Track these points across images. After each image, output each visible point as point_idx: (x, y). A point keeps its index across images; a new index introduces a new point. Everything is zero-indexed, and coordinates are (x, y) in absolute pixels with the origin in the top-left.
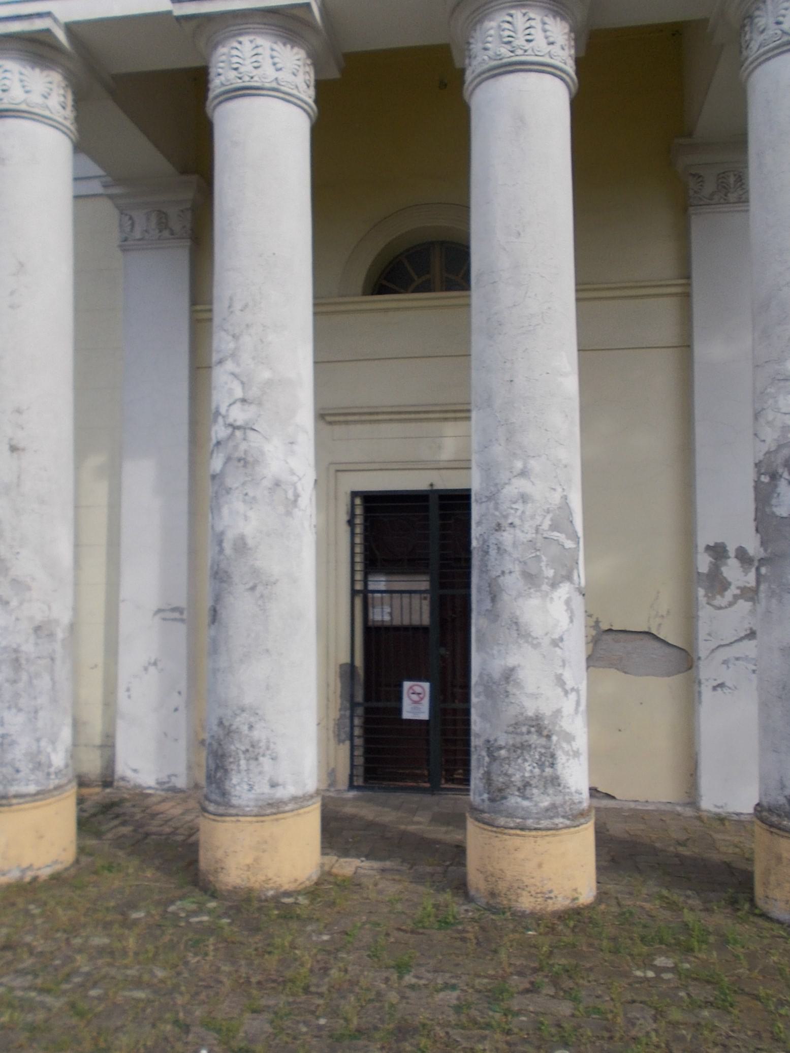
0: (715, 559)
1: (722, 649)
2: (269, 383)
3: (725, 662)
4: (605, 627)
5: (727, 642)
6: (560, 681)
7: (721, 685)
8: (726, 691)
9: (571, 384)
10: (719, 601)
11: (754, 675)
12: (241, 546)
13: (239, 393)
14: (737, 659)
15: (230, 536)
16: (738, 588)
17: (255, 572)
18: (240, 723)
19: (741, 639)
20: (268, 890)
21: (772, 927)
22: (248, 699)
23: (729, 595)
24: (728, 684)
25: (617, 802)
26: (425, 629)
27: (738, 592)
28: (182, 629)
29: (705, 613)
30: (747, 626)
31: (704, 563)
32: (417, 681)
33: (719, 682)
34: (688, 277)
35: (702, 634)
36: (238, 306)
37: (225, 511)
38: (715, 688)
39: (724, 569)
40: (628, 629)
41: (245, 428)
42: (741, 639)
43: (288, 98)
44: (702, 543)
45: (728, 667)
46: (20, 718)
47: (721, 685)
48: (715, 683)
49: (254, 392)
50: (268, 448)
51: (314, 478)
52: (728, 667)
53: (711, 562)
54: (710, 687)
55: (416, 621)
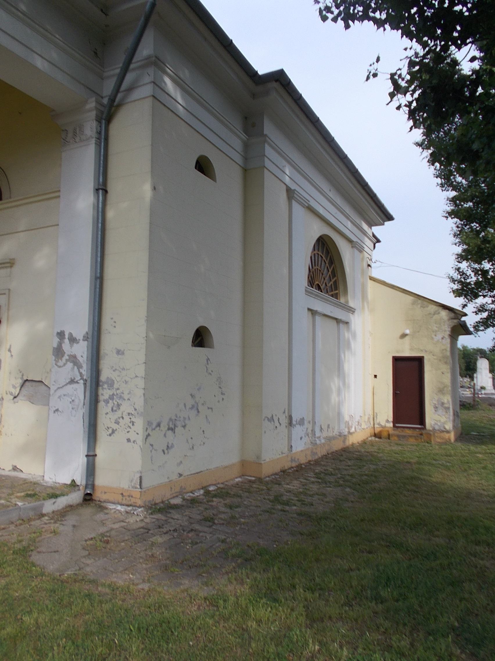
0: (60, 339)
1: (59, 390)
3: (59, 397)
4: (25, 378)
5: (61, 386)
7: (57, 410)
8: (59, 413)
10: (61, 363)
11: (70, 405)
14: (64, 395)
16: (68, 355)
19: (66, 385)
20: (477, 374)
24: (60, 409)
25: (24, 474)
27: (67, 358)
30: (70, 377)
32: (452, 404)
33: (56, 408)
38: (54, 412)
39: (63, 345)
40: (33, 380)
42: (66, 385)
45: (60, 400)
47: (57, 410)
48: (55, 409)
51: (145, 353)
52: (60, 400)
53: (58, 341)
54: (53, 411)
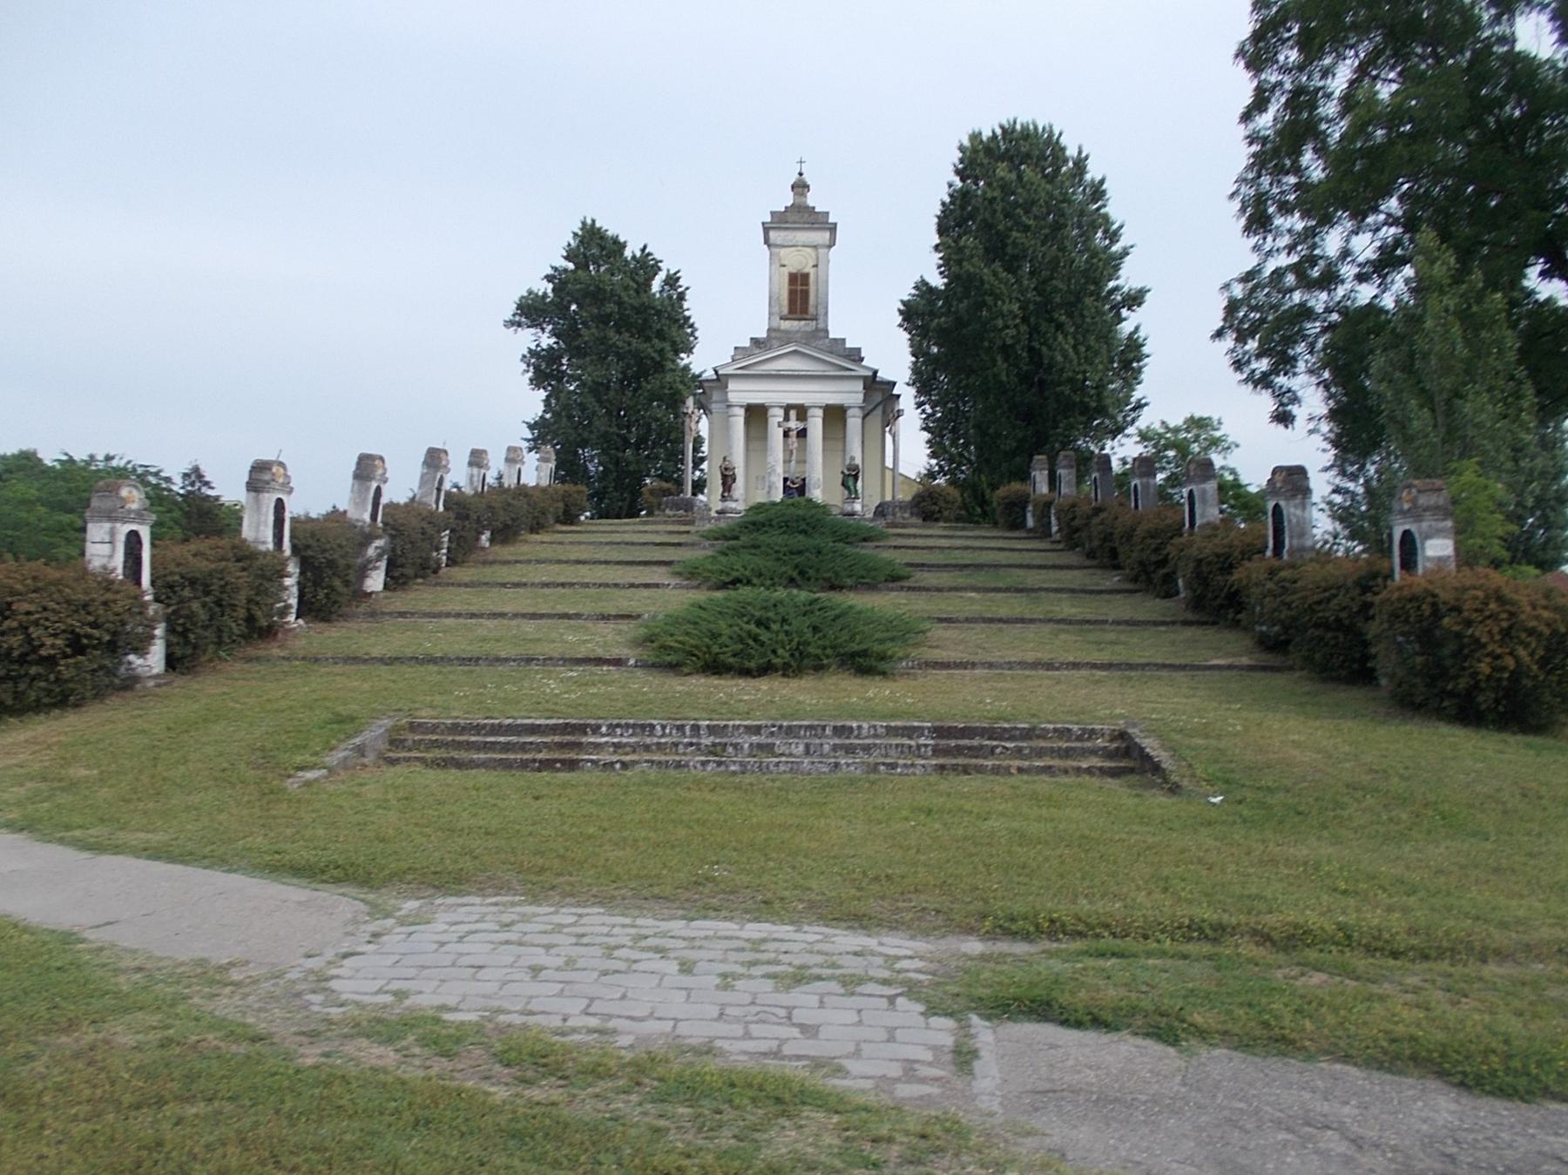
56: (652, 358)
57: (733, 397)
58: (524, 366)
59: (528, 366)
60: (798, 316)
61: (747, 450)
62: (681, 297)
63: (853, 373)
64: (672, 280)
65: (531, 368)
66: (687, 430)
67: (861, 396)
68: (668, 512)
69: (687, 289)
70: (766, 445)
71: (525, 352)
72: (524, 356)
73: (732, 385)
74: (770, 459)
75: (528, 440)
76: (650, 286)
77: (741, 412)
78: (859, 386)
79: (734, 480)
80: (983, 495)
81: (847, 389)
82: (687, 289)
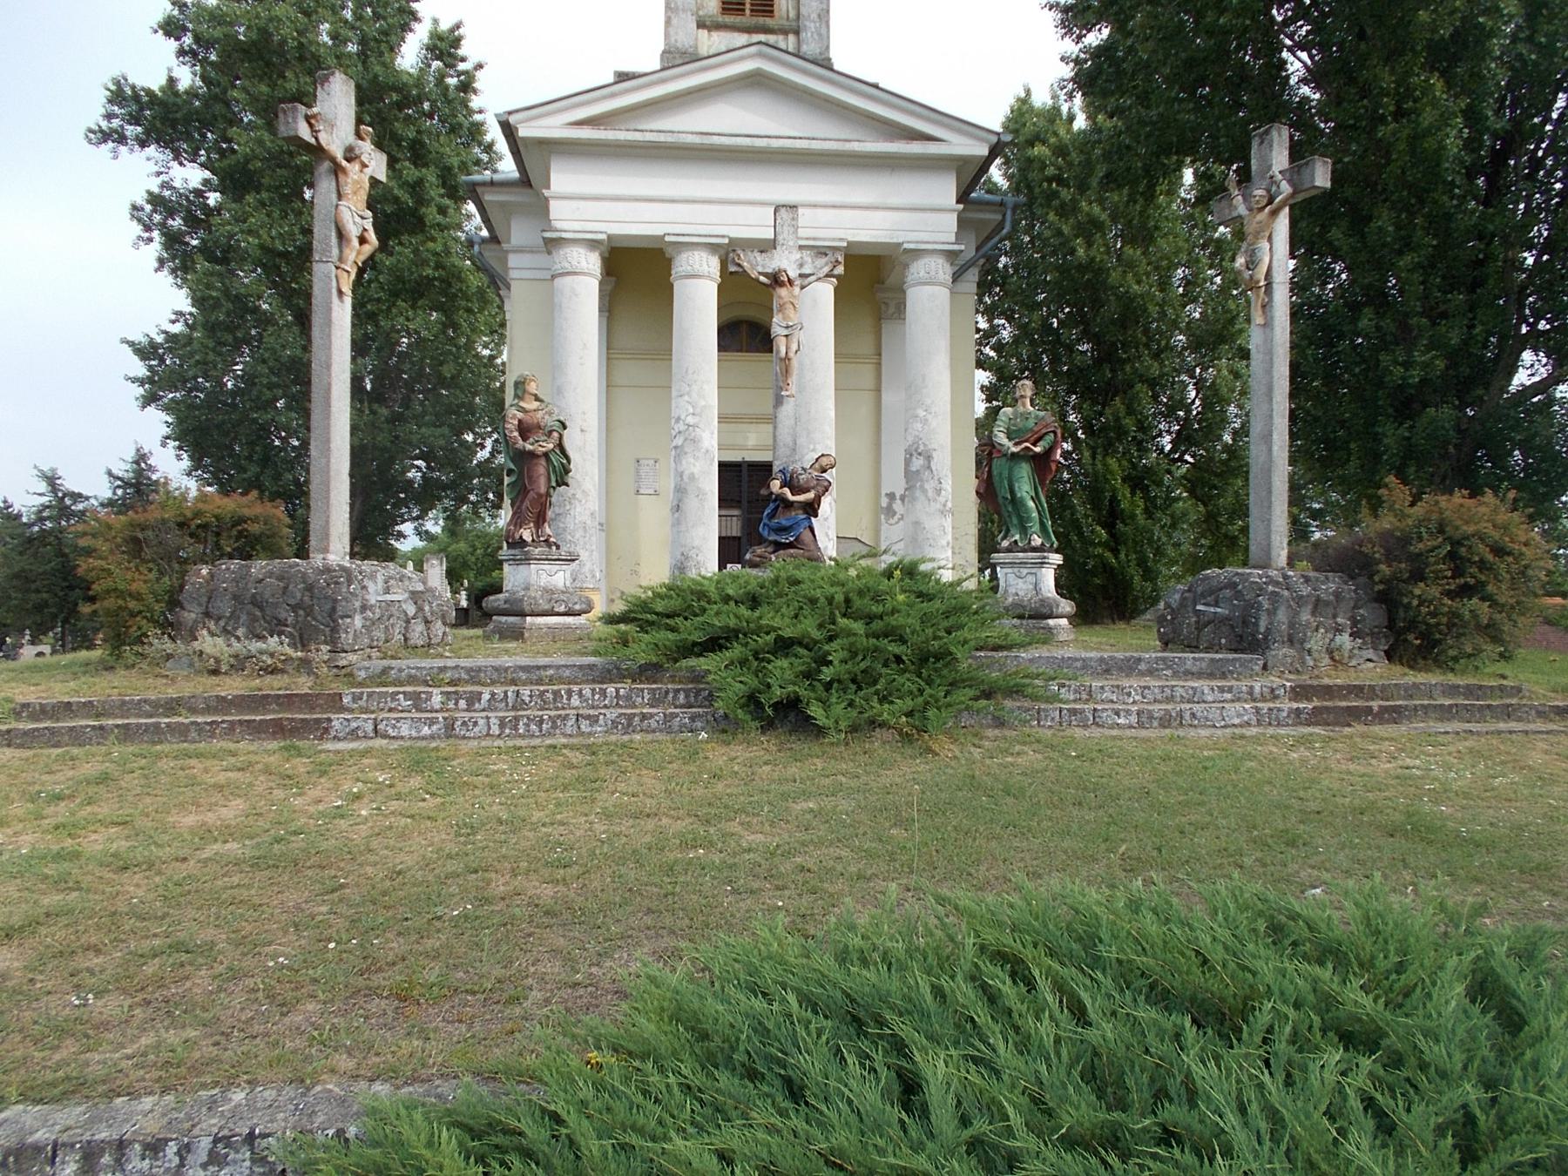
2: (705, 407)
6: (827, 535)
9: (832, 414)
10: (891, 521)
12: (692, 477)
13: (691, 411)
15: (686, 473)
17: (699, 488)
18: (692, 553)
21: (814, 16)
22: (696, 543)
23: (896, 518)
26: (739, 538)
28: (603, 534)
29: (884, 527)
31: (884, 502)
34: (880, 355)
35: (883, 538)
36: (690, 372)
37: (684, 462)
39: (894, 506)
41: (695, 426)
43: (712, 279)
44: (883, 493)
46: (587, 554)
49: (698, 411)
50: (704, 435)
55: (734, 534)
56: (396, 200)
57: (566, 216)
58: (137, 229)
59: (148, 228)
60: (747, 19)
61: (610, 385)
62: (467, 86)
63: (916, 148)
64: (445, 46)
65: (156, 234)
66: (323, 233)
67: (951, 221)
68: (210, 643)
69: (480, 66)
70: (670, 366)
71: (140, 198)
72: (135, 208)
73: (563, 180)
74: (682, 407)
75: (141, 382)
76: (393, 49)
77: (592, 263)
78: (944, 191)
79: (562, 476)
80: (1114, 500)
81: (895, 201)
82: (480, 66)
